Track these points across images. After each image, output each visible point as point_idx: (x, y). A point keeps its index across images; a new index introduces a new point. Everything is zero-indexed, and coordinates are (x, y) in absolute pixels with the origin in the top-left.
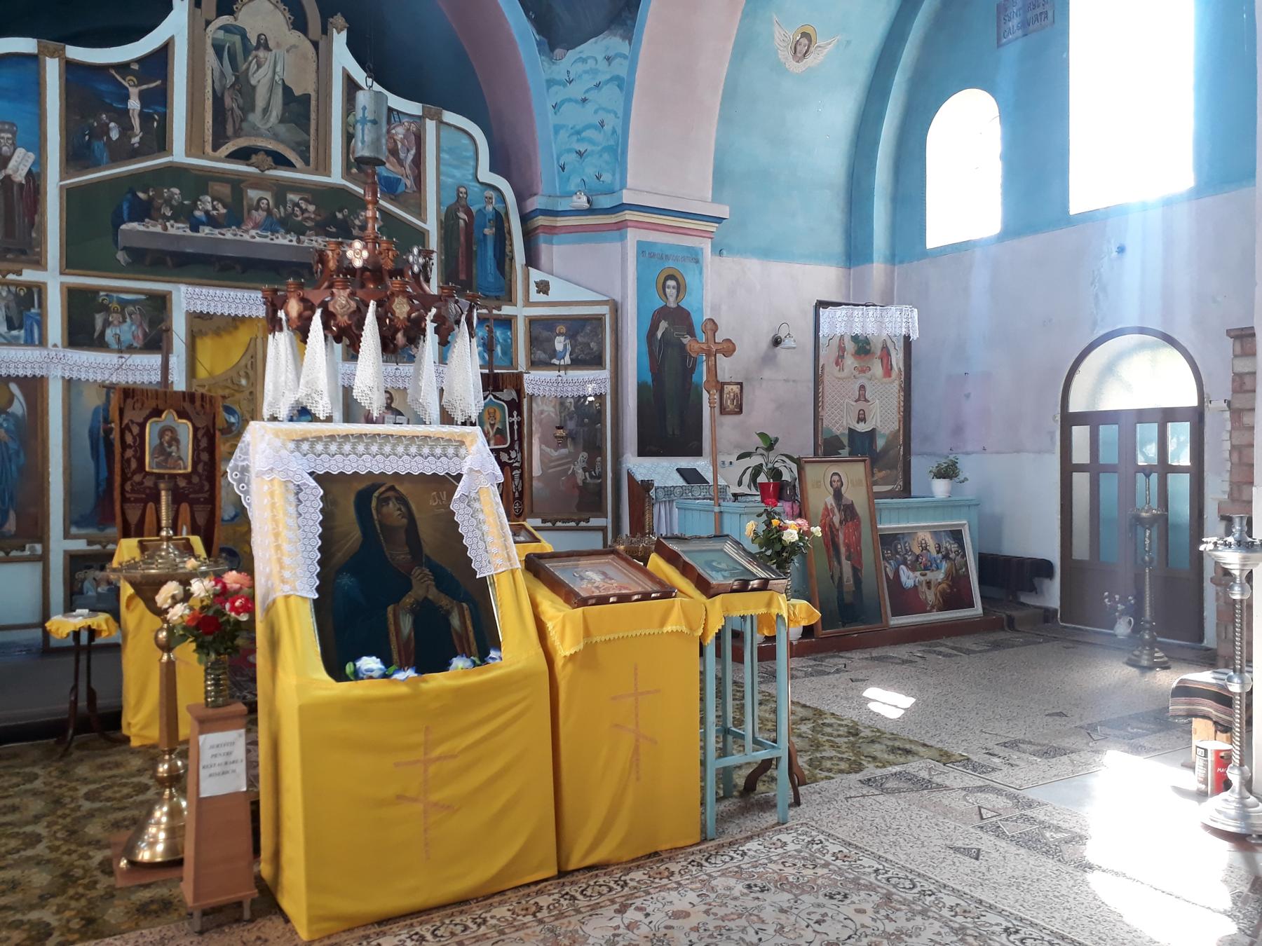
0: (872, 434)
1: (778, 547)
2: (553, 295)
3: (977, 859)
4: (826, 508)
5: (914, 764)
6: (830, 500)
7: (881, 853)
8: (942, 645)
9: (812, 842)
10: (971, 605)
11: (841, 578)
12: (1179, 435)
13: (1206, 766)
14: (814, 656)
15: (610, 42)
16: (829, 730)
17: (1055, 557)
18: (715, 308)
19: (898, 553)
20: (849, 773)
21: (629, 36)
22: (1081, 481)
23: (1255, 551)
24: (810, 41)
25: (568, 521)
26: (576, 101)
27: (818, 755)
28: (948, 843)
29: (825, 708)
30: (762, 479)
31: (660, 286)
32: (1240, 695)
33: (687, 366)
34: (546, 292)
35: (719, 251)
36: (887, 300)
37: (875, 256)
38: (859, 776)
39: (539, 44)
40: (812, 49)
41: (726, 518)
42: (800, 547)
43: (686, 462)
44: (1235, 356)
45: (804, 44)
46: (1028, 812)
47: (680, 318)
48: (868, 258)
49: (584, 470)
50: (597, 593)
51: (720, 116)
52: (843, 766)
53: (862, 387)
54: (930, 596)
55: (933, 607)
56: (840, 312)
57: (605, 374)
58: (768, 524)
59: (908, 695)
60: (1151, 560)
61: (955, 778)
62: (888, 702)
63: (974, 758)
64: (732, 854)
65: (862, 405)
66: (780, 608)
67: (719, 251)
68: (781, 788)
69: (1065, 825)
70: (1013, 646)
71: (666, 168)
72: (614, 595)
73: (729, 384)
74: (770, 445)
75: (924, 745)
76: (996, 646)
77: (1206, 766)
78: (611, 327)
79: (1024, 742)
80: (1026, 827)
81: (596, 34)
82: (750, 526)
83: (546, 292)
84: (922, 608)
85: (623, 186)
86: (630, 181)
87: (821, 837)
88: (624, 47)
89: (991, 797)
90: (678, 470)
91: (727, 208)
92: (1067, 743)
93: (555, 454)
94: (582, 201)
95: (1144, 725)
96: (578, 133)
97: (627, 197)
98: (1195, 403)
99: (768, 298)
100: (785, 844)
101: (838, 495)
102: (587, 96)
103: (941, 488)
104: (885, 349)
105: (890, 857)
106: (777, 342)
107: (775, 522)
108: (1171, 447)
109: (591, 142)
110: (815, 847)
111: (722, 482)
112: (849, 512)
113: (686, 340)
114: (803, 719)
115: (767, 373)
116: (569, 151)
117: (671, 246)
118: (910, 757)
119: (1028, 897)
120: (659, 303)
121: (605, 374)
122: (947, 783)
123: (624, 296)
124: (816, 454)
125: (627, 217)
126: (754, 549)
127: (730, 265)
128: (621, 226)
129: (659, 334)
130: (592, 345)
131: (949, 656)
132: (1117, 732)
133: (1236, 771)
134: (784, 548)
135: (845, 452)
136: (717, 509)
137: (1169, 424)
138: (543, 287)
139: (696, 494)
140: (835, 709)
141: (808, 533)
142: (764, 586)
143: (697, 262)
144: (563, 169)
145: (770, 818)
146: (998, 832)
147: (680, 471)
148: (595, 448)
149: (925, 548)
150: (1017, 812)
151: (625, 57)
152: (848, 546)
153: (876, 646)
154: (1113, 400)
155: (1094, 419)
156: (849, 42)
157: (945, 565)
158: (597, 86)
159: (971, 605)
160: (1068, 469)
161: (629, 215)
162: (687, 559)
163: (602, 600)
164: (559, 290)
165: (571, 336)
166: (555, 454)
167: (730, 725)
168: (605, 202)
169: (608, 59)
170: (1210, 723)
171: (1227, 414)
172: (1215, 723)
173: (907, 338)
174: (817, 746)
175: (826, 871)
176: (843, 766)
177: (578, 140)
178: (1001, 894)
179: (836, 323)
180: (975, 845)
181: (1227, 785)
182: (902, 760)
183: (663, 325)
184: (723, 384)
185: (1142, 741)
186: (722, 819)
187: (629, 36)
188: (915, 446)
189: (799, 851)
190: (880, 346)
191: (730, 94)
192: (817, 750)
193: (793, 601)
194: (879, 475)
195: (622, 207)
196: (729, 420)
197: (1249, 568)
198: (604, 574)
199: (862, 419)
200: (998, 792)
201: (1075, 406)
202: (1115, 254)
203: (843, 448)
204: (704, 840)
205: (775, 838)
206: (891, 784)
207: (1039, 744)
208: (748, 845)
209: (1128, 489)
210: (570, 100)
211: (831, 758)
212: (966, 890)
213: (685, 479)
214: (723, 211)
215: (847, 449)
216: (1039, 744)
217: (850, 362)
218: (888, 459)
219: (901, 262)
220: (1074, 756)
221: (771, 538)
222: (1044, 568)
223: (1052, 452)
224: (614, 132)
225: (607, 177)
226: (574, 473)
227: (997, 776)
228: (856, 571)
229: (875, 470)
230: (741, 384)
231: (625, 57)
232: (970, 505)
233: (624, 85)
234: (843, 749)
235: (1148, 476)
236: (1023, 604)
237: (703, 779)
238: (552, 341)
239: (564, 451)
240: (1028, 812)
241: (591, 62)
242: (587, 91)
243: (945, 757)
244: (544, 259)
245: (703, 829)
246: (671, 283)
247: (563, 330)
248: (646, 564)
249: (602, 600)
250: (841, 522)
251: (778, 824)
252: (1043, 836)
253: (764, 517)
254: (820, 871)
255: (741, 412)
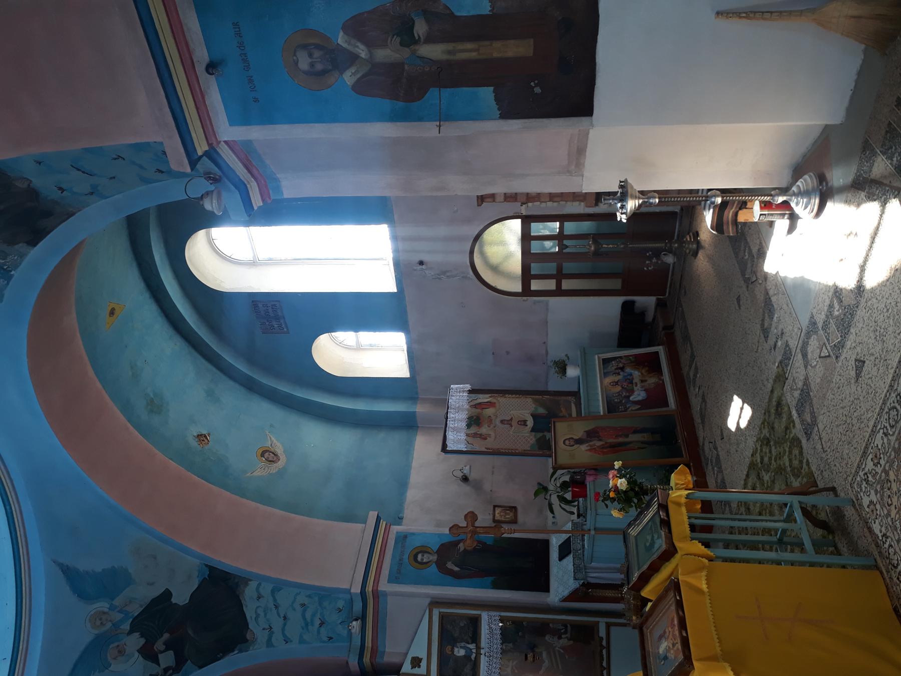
0: (534, 416)
1: (631, 494)
2: (423, 655)
3: (864, 362)
4: (590, 450)
5: (789, 401)
6: (584, 447)
7: (869, 430)
8: (688, 374)
9: (867, 481)
10: (657, 353)
11: (642, 442)
12: (538, 229)
13: (772, 215)
14: (704, 464)
15: (248, 593)
16: (766, 459)
17: (618, 301)
18: (439, 524)
19: (621, 401)
20: (801, 447)
21: (246, 581)
22: (566, 285)
23: (627, 192)
24: (266, 451)
25: (602, 656)
26: (285, 625)
27: (789, 469)
28: (853, 381)
29: (748, 461)
30: (568, 496)
31: (425, 566)
32: (723, 197)
33: (482, 549)
34: (420, 660)
35: (399, 520)
36: (444, 403)
37: (412, 410)
38: (804, 441)
39: (241, 651)
40: (272, 450)
41: (598, 525)
42: (631, 477)
43: (554, 554)
44: (494, 201)
45: (268, 455)
46: (820, 325)
47: (446, 551)
48: (414, 414)
49: (560, 638)
50: (679, 646)
51: (308, 516)
52: (796, 451)
53: (502, 422)
54: (652, 381)
55: (660, 379)
56: (450, 436)
57: (485, 616)
58: (613, 500)
59: (732, 400)
60: (623, 244)
61: (797, 371)
62: (739, 414)
63: (779, 358)
64: (886, 546)
65: (514, 423)
66: (680, 496)
67: (399, 520)
68: (822, 501)
69: (827, 302)
70: (686, 327)
71: (338, 558)
72: (681, 633)
73: (494, 516)
74: (543, 489)
75: (772, 391)
76: (686, 338)
77: (772, 215)
78: (452, 608)
79: (762, 325)
80: (833, 326)
81: (240, 606)
82: (615, 514)
83: (420, 660)
84: (662, 386)
85: (348, 591)
86: (346, 586)
87: (861, 473)
88: (253, 585)
89: (810, 349)
90: (560, 560)
91: (371, 513)
92: (761, 297)
93: (547, 663)
94: (356, 625)
95: (742, 249)
96: (307, 625)
97: (356, 589)
98: (519, 221)
99: (432, 486)
100: (871, 502)
101: (579, 442)
102: (282, 615)
103: (572, 372)
104: (475, 406)
105: (871, 424)
106: (465, 479)
107: (612, 495)
108: (547, 233)
109: (314, 615)
110: (870, 478)
111: (569, 527)
112: (591, 434)
113: (461, 546)
114: (759, 477)
115: (487, 487)
116: (319, 632)
117: (393, 556)
118: (784, 402)
119: (891, 329)
120: (434, 568)
121: (485, 616)
122: (802, 378)
123: (426, 595)
124: (550, 456)
125: (370, 590)
126: (633, 512)
127: (409, 513)
128: (376, 594)
129: (456, 569)
130: (462, 625)
131: (696, 369)
132: (749, 265)
133: (776, 198)
134: (632, 489)
135: (548, 435)
136: (593, 532)
137: (532, 234)
138: (416, 662)
139: (579, 547)
140: (748, 453)
141: (619, 470)
142: (664, 507)
143: (405, 537)
144: (331, 638)
145: (849, 512)
146: (840, 346)
147: (561, 558)
148: (542, 629)
149: (617, 383)
150: (821, 332)
151: (259, 585)
152: (617, 437)
153: (692, 419)
154: (515, 264)
155: (527, 275)
156: (272, 426)
157: (628, 370)
158: (276, 607)
159: (657, 353)
160: (559, 292)
161: (369, 588)
162: (645, 567)
163: (685, 643)
164: (419, 649)
165: (454, 642)
166: (547, 663)
167: (774, 539)
168: (358, 606)
169: (259, 598)
170: (740, 212)
171: (530, 204)
172: (740, 209)
173: (470, 392)
174: (780, 470)
175: (891, 473)
176: (796, 451)
177: (312, 625)
178: (891, 347)
179: (457, 439)
180: (852, 362)
181: (786, 205)
182: (786, 409)
183: (450, 565)
184: (494, 521)
185: (755, 250)
186: (855, 550)
187: (246, 581)
188: (541, 387)
189: (876, 492)
190: (474, 410)
191: (292, 508)
192: (785, 470)
193: (672, 484)
194: (564, 412)
195: (363, 593)
196: (521, 518)
197: (637, 194)
198: (661, 637)
199: (524, 423)
200: (805, 345)
201: (517, 287)
202: (424, 267)
203: (544, 436)
204: (877, 567)
205: (867, 510)
206: (808, 418)
207: (764, 315)
208: (877, 531)
209: (574, 257)
210: (283, 630)
211: (790, 460)
212: (892, 371)
213: (567, 555)
214: (372, 516)
215: (546, 433)
216: (764, 315)
217: (484, 430)
218: (551, 409)
219: (417, 393)
220: (771, 293)
221: (624, 499)
222: (627, 307)
223: (547, 303)
224: (309, 596)
225: (340, 604)
226: (563, 648)
227: (793, 344)
228: (636, 432)
229: (561, 414)
230: (495, 507)
231: (259, 585)
232: (584, 353)
233: (279, 586)
234: (782, 450)
235: (567, 247)
236: (654, 319)
237: (821, 565)
238: (457, 658)
239: (544, 655)
240: (820, 325)
241: (260, 611)
242: (279, 615)
243: (781, 378)
244: (395, 660)
245: (864, 567)
246: (420, 557)
247: (449, 647)
248: (651, 601)
249: (685, 643)
250: (600, 440)
251: (854, 506)
252: (838, 316)
253: (608, 502)
254: (892, 476)
255: (515, 508)
